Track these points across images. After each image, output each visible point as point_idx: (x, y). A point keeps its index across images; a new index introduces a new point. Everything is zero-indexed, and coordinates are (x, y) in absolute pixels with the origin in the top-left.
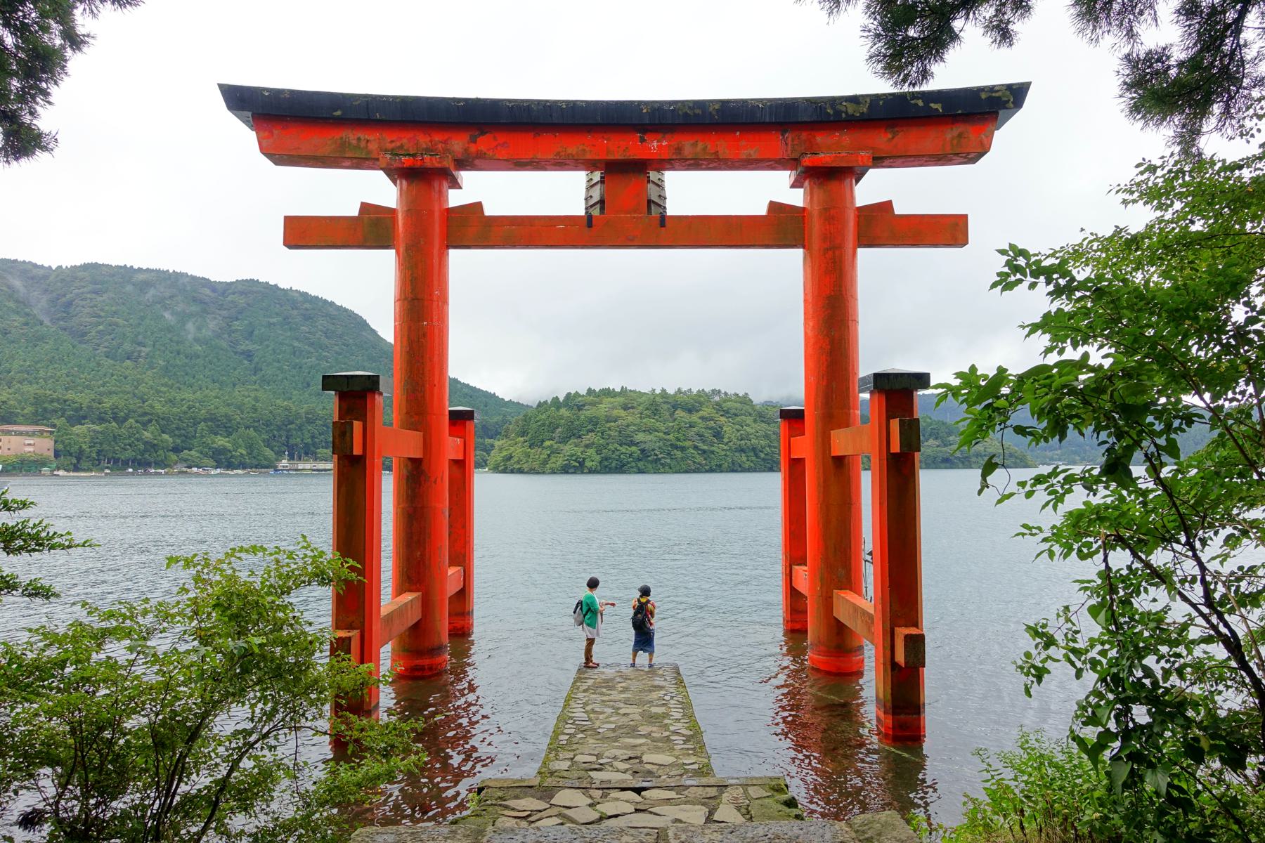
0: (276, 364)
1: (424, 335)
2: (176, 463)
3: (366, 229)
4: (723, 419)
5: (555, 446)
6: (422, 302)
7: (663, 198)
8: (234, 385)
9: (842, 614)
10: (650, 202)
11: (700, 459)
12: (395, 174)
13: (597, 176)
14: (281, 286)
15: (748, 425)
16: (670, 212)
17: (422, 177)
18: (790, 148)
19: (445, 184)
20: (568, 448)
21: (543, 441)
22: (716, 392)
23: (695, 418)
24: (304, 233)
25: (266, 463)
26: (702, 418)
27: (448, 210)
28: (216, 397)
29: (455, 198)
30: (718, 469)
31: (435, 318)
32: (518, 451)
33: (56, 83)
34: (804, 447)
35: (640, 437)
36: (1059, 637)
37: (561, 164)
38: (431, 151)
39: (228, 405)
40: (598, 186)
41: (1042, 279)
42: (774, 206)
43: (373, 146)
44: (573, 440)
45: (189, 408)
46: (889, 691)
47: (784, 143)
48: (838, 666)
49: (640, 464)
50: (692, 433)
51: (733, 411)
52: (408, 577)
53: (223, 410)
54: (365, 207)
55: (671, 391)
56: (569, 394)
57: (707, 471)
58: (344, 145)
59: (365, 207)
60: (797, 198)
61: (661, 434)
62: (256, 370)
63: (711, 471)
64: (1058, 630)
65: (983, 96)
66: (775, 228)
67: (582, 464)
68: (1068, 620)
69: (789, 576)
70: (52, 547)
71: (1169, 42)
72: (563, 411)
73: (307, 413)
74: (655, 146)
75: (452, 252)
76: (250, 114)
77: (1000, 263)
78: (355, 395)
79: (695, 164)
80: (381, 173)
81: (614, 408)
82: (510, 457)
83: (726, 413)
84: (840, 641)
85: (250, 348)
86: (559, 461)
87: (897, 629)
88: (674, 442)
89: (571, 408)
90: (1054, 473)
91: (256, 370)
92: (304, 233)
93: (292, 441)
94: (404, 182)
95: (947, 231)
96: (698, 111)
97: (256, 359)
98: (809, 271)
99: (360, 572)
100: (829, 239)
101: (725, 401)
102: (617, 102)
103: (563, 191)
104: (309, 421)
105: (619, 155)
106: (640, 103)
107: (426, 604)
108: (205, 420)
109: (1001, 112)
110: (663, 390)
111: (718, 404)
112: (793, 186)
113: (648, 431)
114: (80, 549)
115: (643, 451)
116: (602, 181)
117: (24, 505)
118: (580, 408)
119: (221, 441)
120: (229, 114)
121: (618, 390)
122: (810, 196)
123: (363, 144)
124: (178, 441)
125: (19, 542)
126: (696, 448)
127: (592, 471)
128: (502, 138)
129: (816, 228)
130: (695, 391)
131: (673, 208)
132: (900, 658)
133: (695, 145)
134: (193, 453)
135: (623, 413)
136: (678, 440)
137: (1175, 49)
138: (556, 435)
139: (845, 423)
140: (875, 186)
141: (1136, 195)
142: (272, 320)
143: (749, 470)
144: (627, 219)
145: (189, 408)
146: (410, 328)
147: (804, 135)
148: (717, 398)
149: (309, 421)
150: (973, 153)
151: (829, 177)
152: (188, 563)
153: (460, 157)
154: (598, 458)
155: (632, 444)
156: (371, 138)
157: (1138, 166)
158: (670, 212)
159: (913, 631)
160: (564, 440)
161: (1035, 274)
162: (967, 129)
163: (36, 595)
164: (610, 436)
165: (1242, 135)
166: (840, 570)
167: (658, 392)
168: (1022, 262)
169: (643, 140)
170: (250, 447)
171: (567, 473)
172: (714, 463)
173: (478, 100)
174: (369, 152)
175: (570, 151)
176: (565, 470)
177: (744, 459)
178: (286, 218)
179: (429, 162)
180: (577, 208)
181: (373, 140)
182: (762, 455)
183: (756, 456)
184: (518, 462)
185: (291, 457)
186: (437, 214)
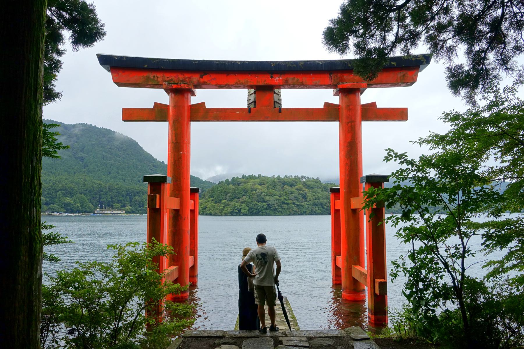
0: (95, 163)
1: (181, 158)
2: (47, 211)
3: (157, 113)
4: (307, 190)
5: (227, 203)
6: (179, 145)
8: (75, 173)
9: (355, 275)
10: (275, 102)
11: (295, 209)
12: (168, 91)
13: (252, 91)
14: (98, 126)
15: (318, 193)
16: (283, 106)
17: (180, 92)
18: (333, 80)
19: (189, 95)
20: (233, 204)
21: (221, 200)
22: (303, 177)
23: (293, 189)
24: (130, 115)
25: (89, 210)
26: (297, 189)
27: (191, 106)
28: (66, 179)
29: (194, 100)
30: (305, 213)
31: (185, 150)
32: (209, 205)
33: (58, 72)
34: (340, 205)
35: (267, 198)
36: (401, 265)
37: (237, 86)
38: (184, 81)
39: (72, 183)
40: (253, 95)
41: (398, 158)
42: (327, 104)
43: (160, 79)
44: (236, 200)
45: (54, 184)
46: (373, 305)
47: (328, 78)
48: (356, 302)
49: (268, 211)
50: (292, 196)
51: (312, 186)
52: (173, 259)
53: (70, 185)
54: (156, 104)
55: (282, 176)
56: (233, 178)
57: (299, 215)
58: (148, 79)
59: (156, 104)
60: (336, 100)
61: (277, 197)
62: (85, 166)
63: (301, 214)
64: (400, 262)
65: (413, 59)
66: (328, 113)
67: (240, 211)
68: (403, 259)
69: (334, 260)
70: (59, 243)
71: (463, 63)
72: (231, 186)
73: (109, 187)
74: (277, 79)
75: (192, 123)
76: (109, 66)
77: (385, 154)
78: (156, 184)
79: (294, 86)
80: (162, 90)
81: (255, 184)
82: (206, 208)
83: (308, 187)
84: (355, 286)
85: (83, 155)
86: (229, 209)
87: (376, 280)
88: (283, 200)
89: (234, 184)
90: (393, 217)
91: (85, 166)
92: (130, 115)
93: (102, 200)
94: (173, 94)
95: (399, 114)
96: (295, 65)
97: (85, 161)
98: (341, 131)
100: (350, 117)
101: (308, 181)
102: (261, 62)
103: (239, 98)
104: (110, 190)
106: (271, 62)
107: (181, 271)
108: (61, 190)
109: (421, 66)
110: (278, 176)
111: (304, 182)
112: (335, 95)
113: (271, 195)
114: (68, 244)
115: (268, 205)
116: (255, 93)
117: (52, 227)
118: (239, 184)
119: (68, 200)
120: (101, 67)
121: (257, 176)
122: (341, 100)
123: (156, 78)
124: (48, 200)
125: (48, 241)
126: (294, 203)
127: (244, 215)
128: (213, 76)
129: (344, 113)
130: (293, 176)
131: (285, 105)
132: (377, 291)
133: (294, 79)
134: (55, 205)
135: (259, 187)
136: (286, 200)
137: (465, 65)
138: (228, 197)
139: (357, 195)
140: (370, 96)
141: (447, 120)
142: (93, 143)
143: (319, 214)
144: (265, 108)
145: (54, 184)
146: (175, 155)
147: (339, 75)
148: (304, 180)
149: (110, 190)
150: (410, 82)
151: (349, 93)
152: (115, 247)
153: (196, 84)
154: (247, 208)
155: (263, 201)
156: (159, 76)
157: (443, 114)
158: (283, 106)
159: (382, 280)
160: (231, 200)
161: (396, 157)
162: (408, 74)
163: (53, 260)
164: (253, 197)
165: (484, 99)
166: (355, 258)
167: (276, 177)
168: (392, 153)
169: (272, 77)
170: (82, 203)
171: (232, 215)
172: (303, 210)
173: (204, 61)
174: (159, 82)
175: (241, 81)
176: (232, 214)
177: (317, 209)
178: (123, 109)
179: (183, 86)
180: (244, 105)
181: (160, 77)
182: (326, 207)
183: (323, 207)
184: (209, 210)
185: (101, 208)
186: (186, 108)
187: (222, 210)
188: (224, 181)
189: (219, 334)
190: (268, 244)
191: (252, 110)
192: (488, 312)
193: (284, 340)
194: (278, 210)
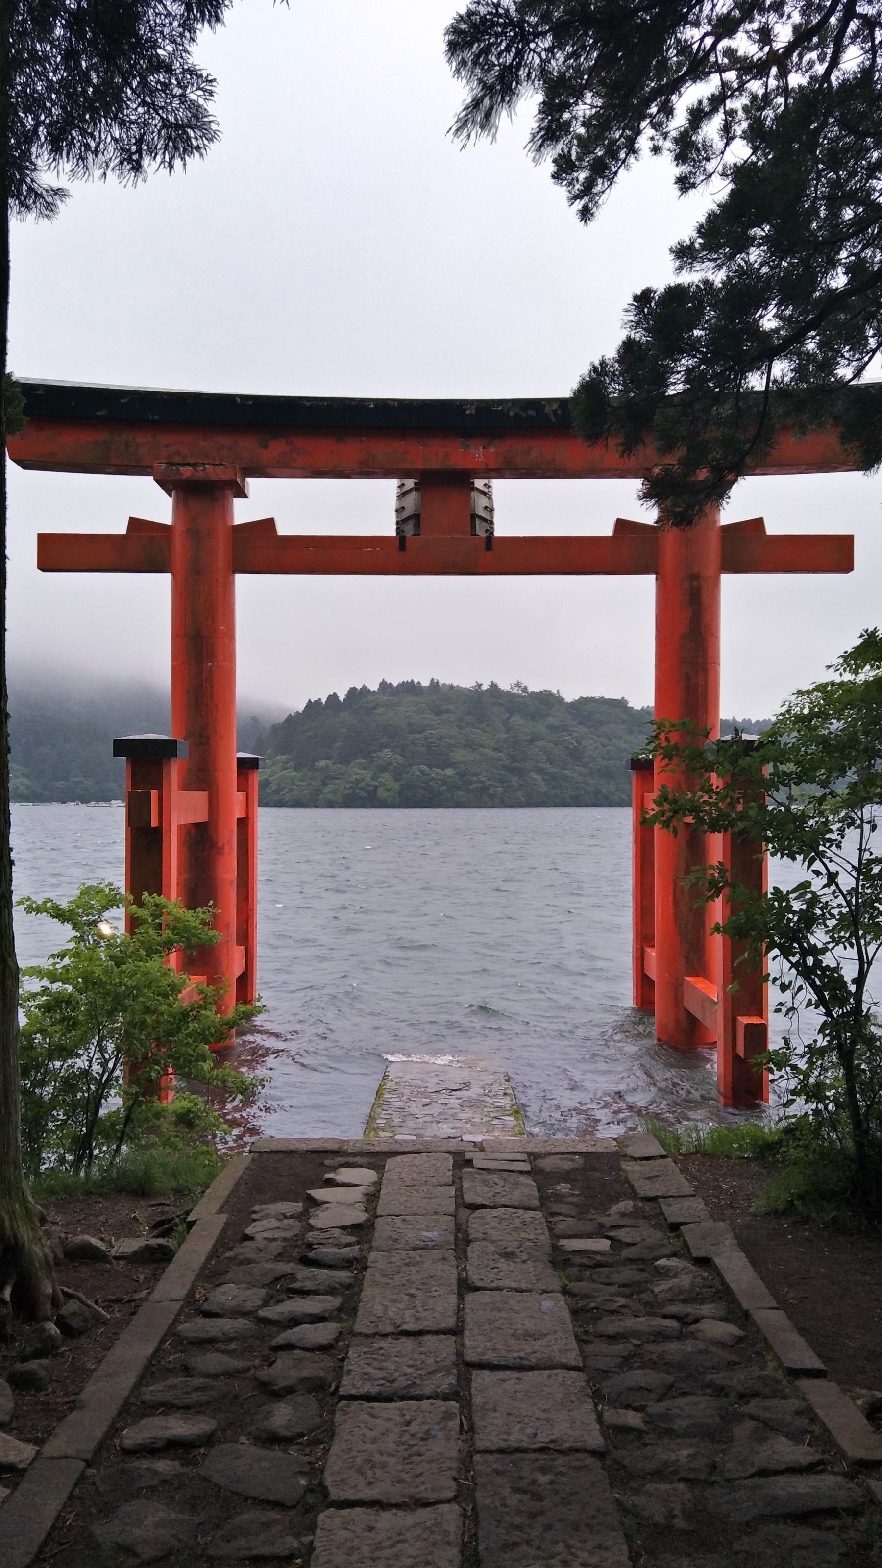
6: (202, 641)
7: (490, 510)
10: (474, 516)
13: (410, 483)
23: (540, 727)
26: (551, 727)
29: (243, 512)
35: (460, 755)
40: (414, 495)
42: (622, 525)
54: (134, 523)
59: (134, 523)
60: (647, 514)
61: (489, 752)
80: (150, 480)
95: (830, 554)
99: (201, 958)
100: (686, 561)
103: (367, 506)
105: (435, 464)
110: (494, 686)
113: (469, 745)
116: (417, 488)
121: (426, 683)
144: (443, 538)
151: (687, 495)
154: (396, 786)
158: (500, 531)
159: (755, 1020)
160: (345, 760)
167: (485, 687)
176: (350, 801)
177: (612, 787)
187: (317, 792)
188: (324, 701)
189: (335, 1147)
190: (677, 171)
191: (408, 543)
192: (830, 1107)
193: (479, 1160)
194: (491, 791)
